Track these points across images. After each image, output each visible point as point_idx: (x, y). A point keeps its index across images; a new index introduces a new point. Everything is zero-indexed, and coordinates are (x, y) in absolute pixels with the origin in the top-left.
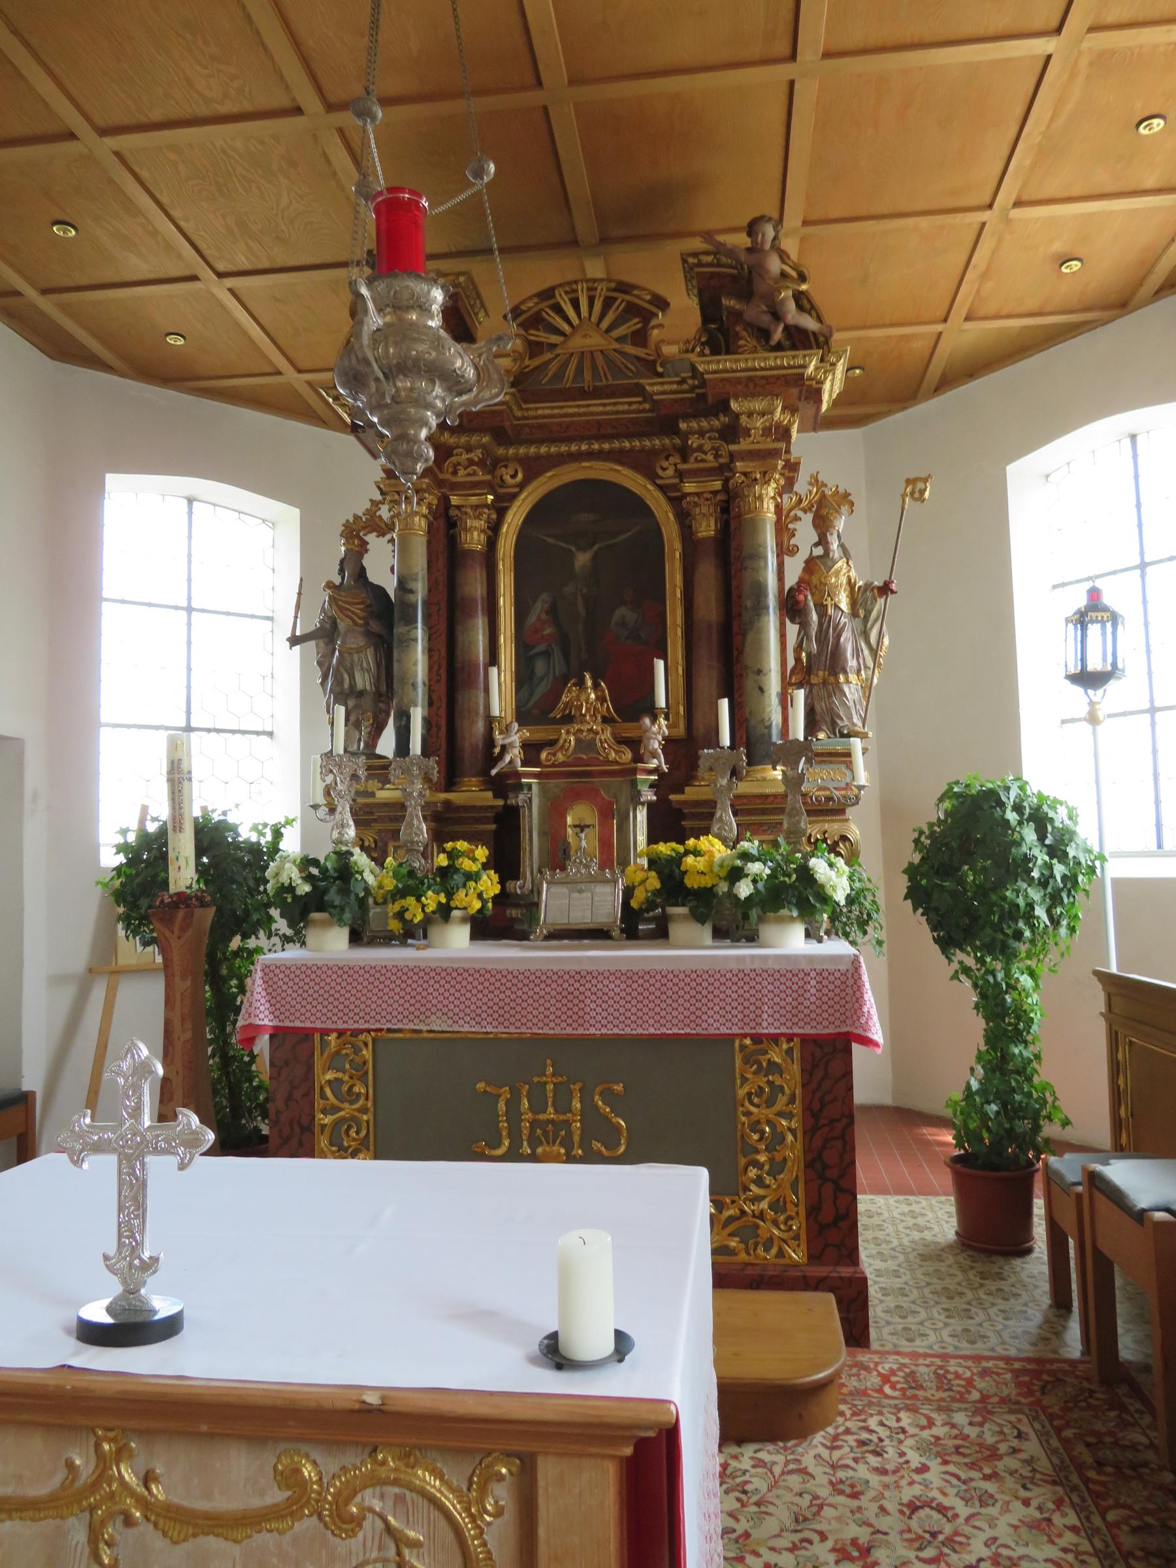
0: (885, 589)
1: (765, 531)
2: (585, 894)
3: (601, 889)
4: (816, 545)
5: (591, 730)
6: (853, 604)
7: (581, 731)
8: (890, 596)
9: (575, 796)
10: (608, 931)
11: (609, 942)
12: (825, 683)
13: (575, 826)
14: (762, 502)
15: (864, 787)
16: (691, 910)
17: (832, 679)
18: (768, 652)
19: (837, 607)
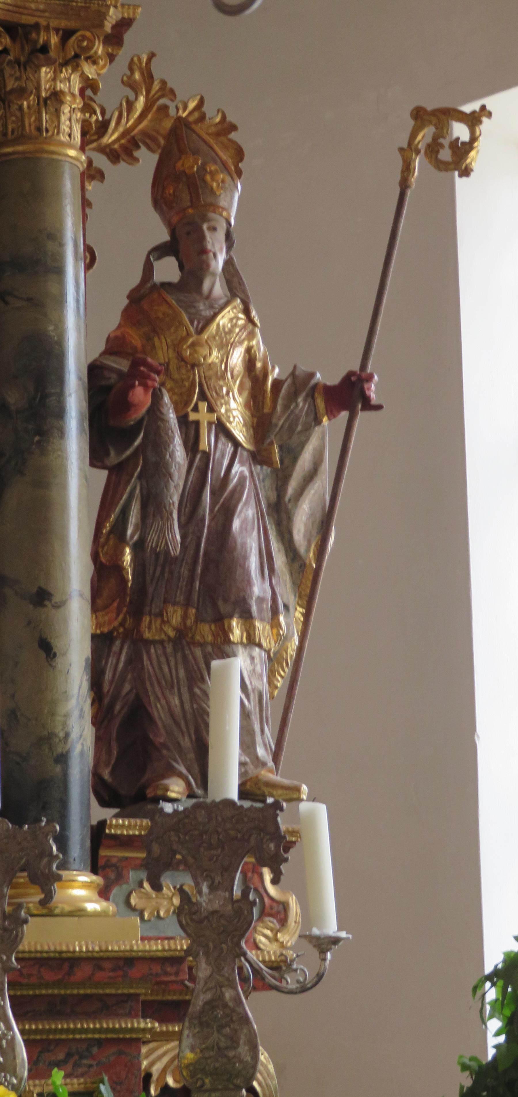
0: (349, 395)
1: (58, 195)
4: (161, 251)
6: (260, 424)
8: (362, 417)
12: (183, 638)
14: (57, 113)
15: (335, 941)
17: (206, 631)
19: (222, 429)
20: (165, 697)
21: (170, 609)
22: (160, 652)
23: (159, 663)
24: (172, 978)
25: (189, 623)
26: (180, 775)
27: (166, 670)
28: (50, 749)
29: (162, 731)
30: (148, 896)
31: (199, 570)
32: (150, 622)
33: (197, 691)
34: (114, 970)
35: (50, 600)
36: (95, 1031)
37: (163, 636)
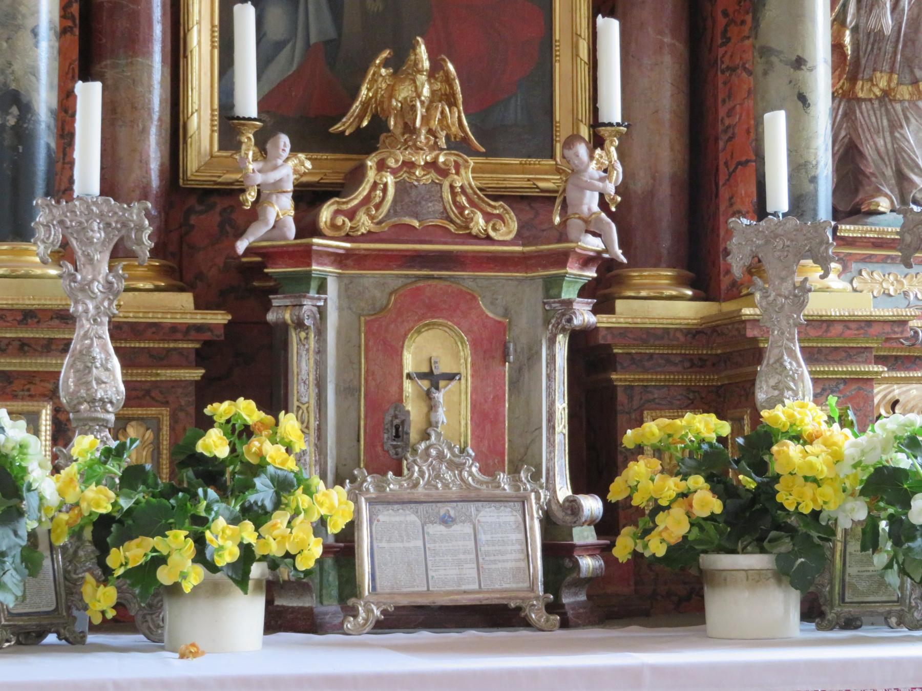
2: (457, 528)
3: (488, 515)
5: (432, 165)
7: (410, 165)
9: (423, 309)
10: (519, 609)
11: (524, 633)
13: (422, 376)
16: (780, 558)
18: (813, 20)
20: (873, 140)
21: (878, 74)
22: (869, 107)
23: (869, 115)
24: (899, 336)
25: (892, 85)
26: (886, 195)
27: (874, 120)
28: (806, 172)
29: (872, 164)
30: (866, 282)
31: (900, 47)
32: (863, 85)
33: (897, 134)
34: (858, 329)
35: (805, 65)
36: (843, 372)
37: (872, 96)
